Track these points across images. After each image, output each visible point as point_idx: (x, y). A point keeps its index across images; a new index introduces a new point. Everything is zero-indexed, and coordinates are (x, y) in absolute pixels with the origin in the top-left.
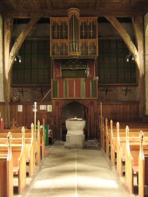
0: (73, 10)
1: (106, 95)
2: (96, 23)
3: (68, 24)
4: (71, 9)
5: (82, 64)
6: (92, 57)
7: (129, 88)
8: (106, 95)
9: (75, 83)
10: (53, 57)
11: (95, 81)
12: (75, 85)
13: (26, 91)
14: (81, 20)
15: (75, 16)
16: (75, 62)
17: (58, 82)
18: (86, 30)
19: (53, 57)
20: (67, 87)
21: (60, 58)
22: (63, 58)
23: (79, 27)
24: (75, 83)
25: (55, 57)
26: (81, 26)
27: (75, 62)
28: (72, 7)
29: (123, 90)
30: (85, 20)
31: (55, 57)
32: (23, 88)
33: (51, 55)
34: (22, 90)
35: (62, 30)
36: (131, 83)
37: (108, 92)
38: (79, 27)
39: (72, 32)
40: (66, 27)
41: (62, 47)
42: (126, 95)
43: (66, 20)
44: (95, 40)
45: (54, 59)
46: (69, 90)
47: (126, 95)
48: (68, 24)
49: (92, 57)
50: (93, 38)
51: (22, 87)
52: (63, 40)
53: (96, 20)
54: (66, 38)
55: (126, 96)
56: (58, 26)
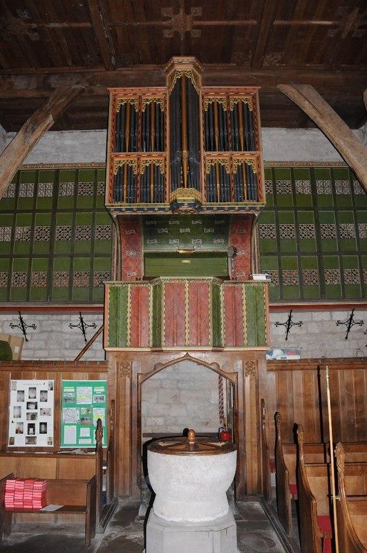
0: (180, 63)
1: (286, 339)
2: (254, 104)
3: (166, 109)
4: (175, 59)
5: (210, 234)
6: (244, 208)
7: (297, 317)
8: (286, 339)
10: (116, 210)
11: (257, 289)
13: (34, 327)
14: (116, 159)
15: (188, 80)
16: (188, 230)
17: (129, 289)
19: (116, 210)
20: (160, 309)
21: (140, 213)
22: (158, 213)
23: (201, 115)
25: (120, 210)
26: (208, 116)
28: (179, 55)
29: (339, 323)
31: (120, 210)
32: (22, 316)
33: (107, 204)
34: (24, 331)
35: (146, 126)
36: (344, 298)
37: (294, 329)
38: (201, 115)
39: (178, 129)
40: (161, 117)
42: (346, 338)
43: (158, 94)
45: (117, 216)
46: (168, 318)
47: (346, 338)
48: (166, 109)
49: (247, 208)
50: (245, 150)
51: (19, 311)
53: (254, 97)
54: (160, 148)
55: (347, 343)
56: (134, 115)
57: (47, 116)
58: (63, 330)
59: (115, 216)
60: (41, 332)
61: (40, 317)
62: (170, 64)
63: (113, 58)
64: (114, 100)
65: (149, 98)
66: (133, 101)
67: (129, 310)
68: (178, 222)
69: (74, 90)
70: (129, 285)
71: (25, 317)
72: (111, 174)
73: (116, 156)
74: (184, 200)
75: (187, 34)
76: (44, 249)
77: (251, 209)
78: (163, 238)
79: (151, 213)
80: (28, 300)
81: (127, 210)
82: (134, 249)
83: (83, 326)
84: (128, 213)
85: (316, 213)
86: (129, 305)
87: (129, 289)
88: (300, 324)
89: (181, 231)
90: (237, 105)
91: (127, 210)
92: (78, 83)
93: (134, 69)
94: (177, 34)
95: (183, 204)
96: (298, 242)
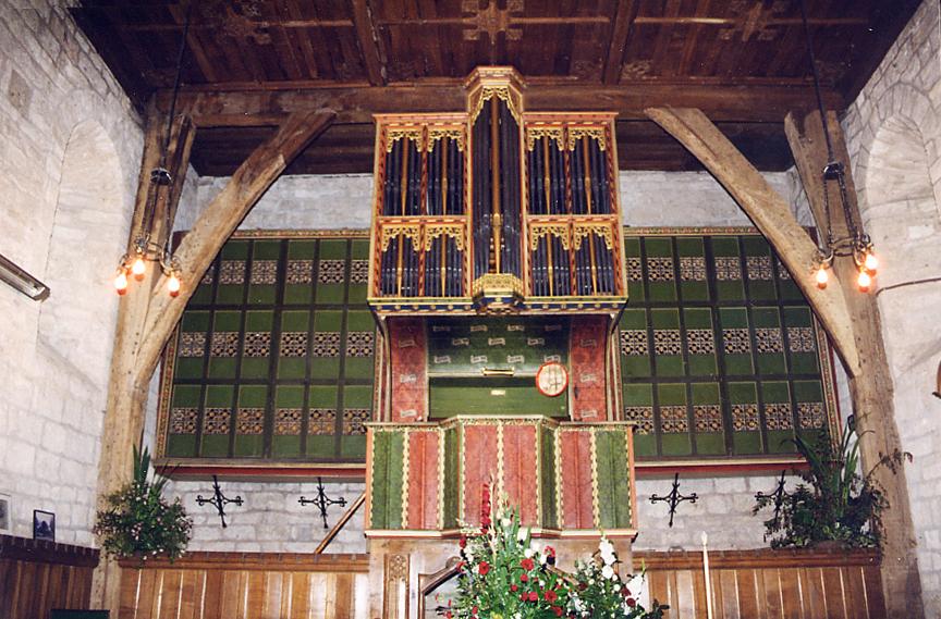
0: (490, 77)
2: (609, 139)
3: (466, 147)
4: (482, 70)
5: (538, 346)
9: (500, 445)
12: (500, 455)
13: (238, 501)
16: (503, 341)
17: (406, 436)
18: (557, 173)
19: (384, 307)
20: (457, 467)
21: (424, 313)
23: (523, 157)
24: (500, 445)
26: (533, 158)
27: (503, 341)
28: (487, 64)
30: (551, 129)
31: (392, 308)
35: (434, 174)
38: (523, 157)
41: (432, 259)
44: (606, 220)
48: (466, 147)
50: (594, 212)
52: (440, 221)
57: (275, 156)
58: (287, 509)
59: (383, 318)
60: (249, 512)
61: (248, 486)
62: (473, 79)
63: (383, 69)
64: (384, 133)
65: (440, 130)
66: (413, 134)
67: (406, 469)
68: (485, 329)
69: (320, 115)
70: (406, 429)
71: (222, 485)
72: (377, 250)
73: (387, 222)
74: (496, 293)
75: (501, 36)
76: (261, 371)
77: (603, 306)
78: (461, 355)
79: (441, 312)
80: (230, 456)
81: (403, 307)
82: (413, 372)
83: (322, 502)
84: (406, 313)
85: (716, 312)
86: (406, 461)
87: (406, 436)
88: (693, 498)
89: (490, 342)
90: (581, 140)
91: (403, 307)
92: (325, 106)
93: (415, 84)
94: (484, 35)
95: (493, 300)
96: (686, 360)
